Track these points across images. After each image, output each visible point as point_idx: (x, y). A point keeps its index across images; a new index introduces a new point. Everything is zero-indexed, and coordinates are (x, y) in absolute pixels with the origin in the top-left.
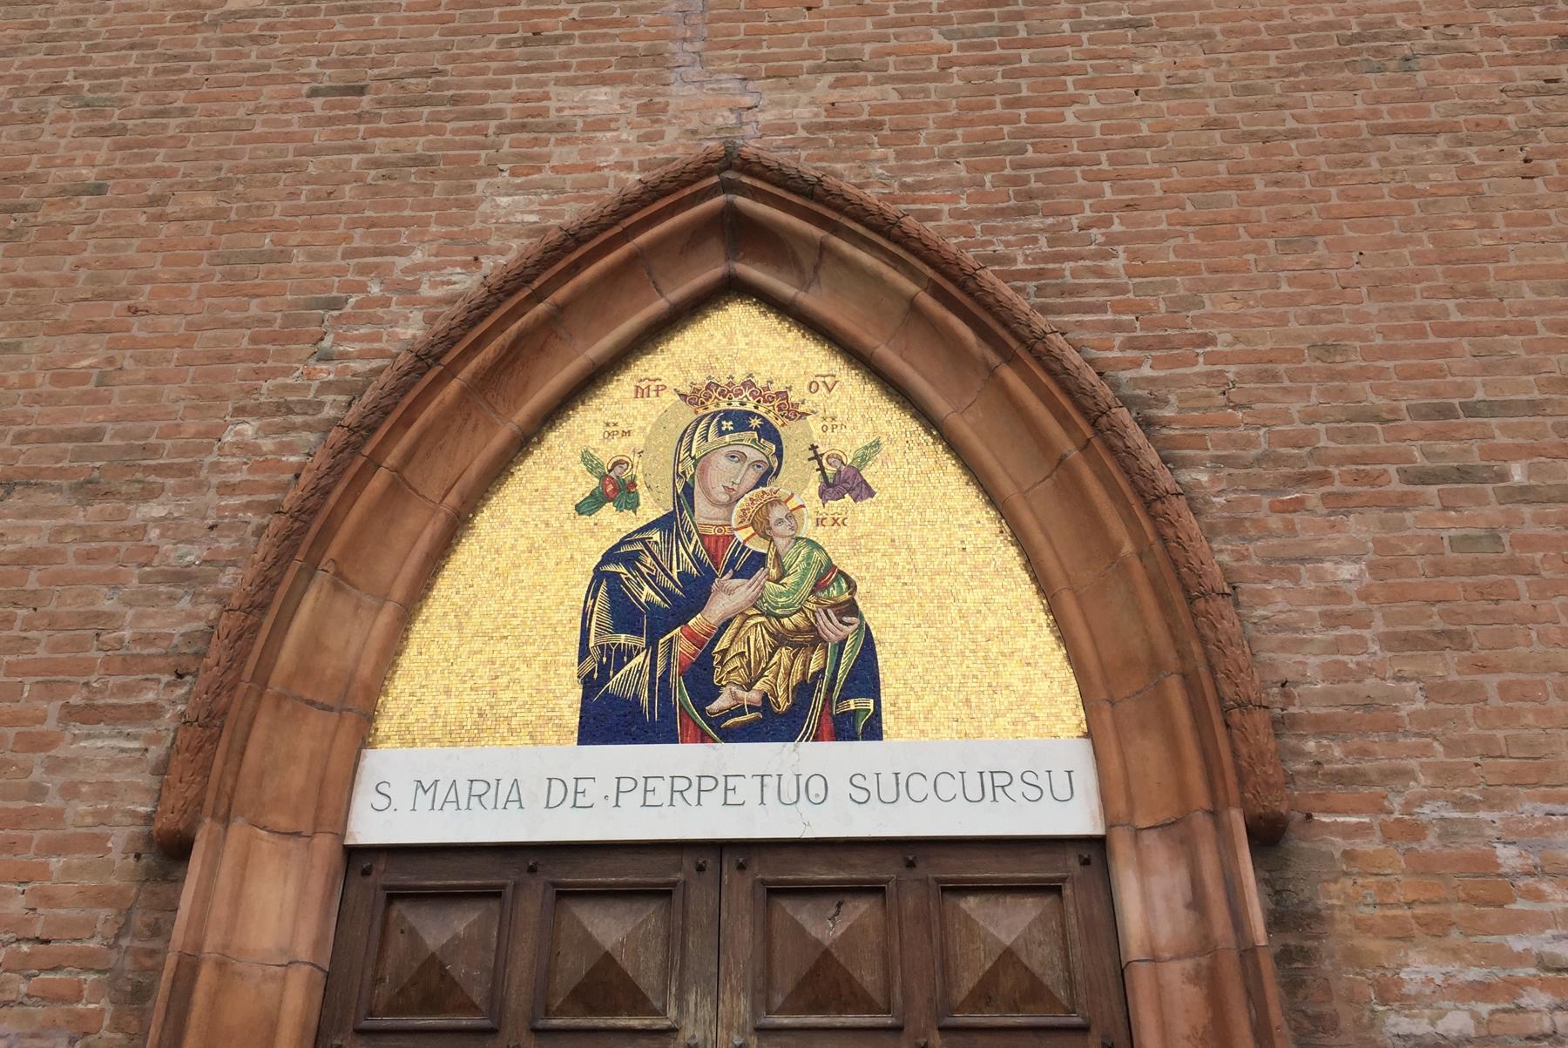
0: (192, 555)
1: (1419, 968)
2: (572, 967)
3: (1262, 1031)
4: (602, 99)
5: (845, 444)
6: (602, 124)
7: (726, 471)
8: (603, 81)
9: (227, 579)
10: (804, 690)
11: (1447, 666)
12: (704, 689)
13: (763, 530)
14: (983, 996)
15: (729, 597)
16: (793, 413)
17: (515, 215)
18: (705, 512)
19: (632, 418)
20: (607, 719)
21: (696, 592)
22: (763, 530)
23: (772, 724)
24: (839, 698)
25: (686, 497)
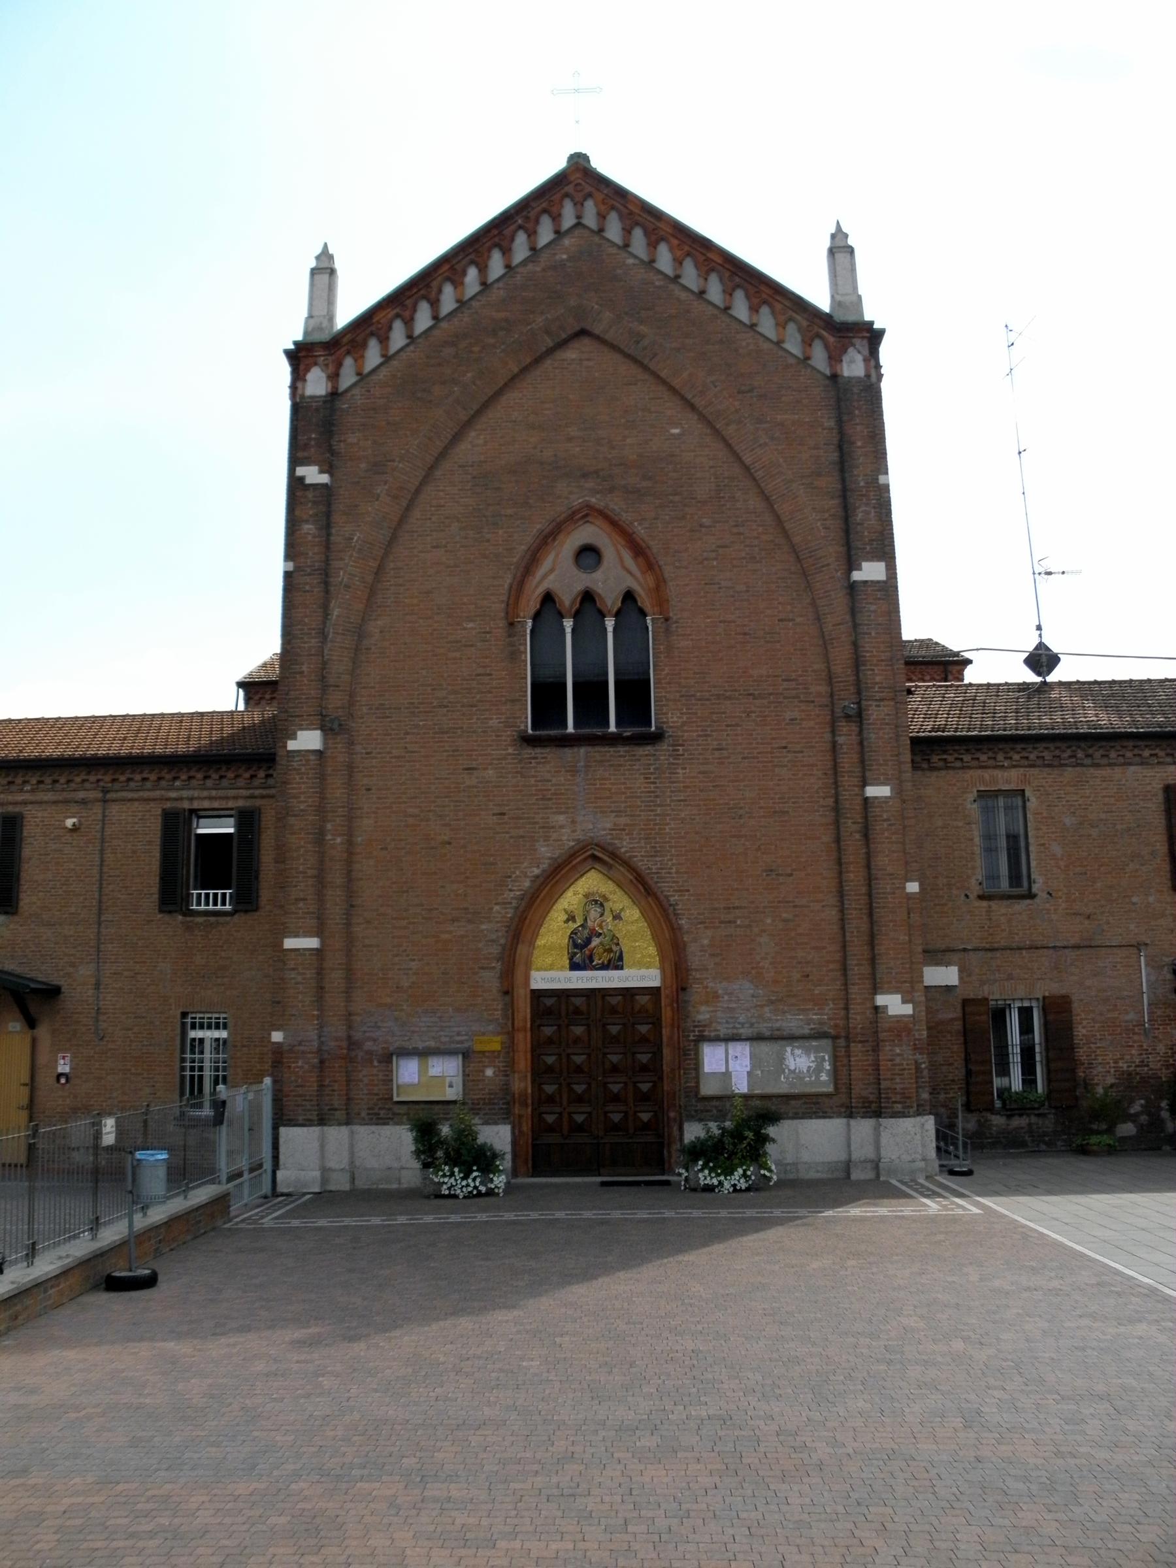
0: (494, 937)
1: (703, 1008)
2: (571, 1008)
3: (2, 804)
4: (561, 819)
5: (617, 907)
6: (562, 827)
7: (594, 913)
8: (561, 813)
9: (502, 941)
10: (610, 961)
11: (717, 960)
12: (592, 961)
13: (600, 926)
14: (639, 1012)
15: (595, 942)
16: (607, 900)
17: (546, 852)
18: (590, 923)
19: (571, 898)
20: (574, 967)
21: (588, 941)
22: (600, 926)
23: (604, 967)
24: (616, 963)
25: (586, 920)
